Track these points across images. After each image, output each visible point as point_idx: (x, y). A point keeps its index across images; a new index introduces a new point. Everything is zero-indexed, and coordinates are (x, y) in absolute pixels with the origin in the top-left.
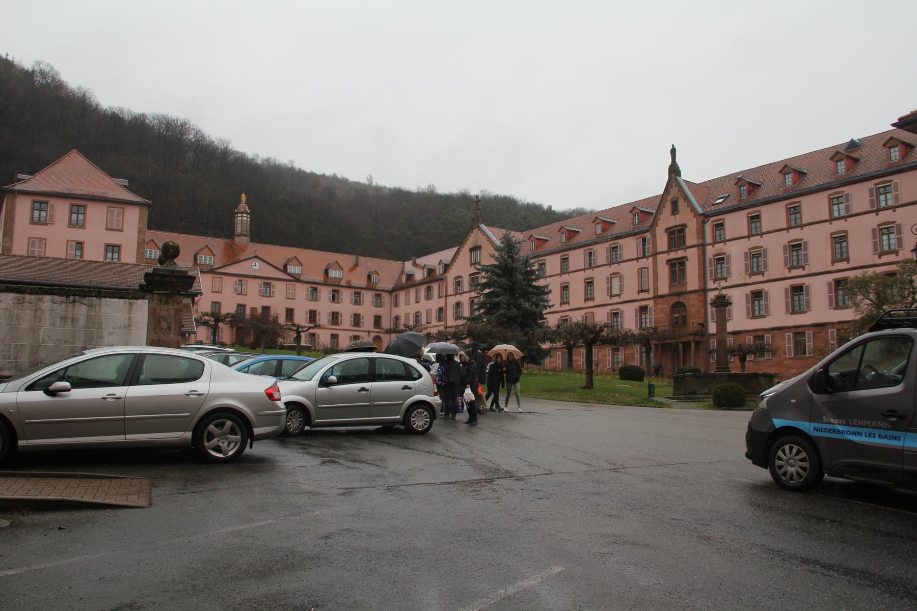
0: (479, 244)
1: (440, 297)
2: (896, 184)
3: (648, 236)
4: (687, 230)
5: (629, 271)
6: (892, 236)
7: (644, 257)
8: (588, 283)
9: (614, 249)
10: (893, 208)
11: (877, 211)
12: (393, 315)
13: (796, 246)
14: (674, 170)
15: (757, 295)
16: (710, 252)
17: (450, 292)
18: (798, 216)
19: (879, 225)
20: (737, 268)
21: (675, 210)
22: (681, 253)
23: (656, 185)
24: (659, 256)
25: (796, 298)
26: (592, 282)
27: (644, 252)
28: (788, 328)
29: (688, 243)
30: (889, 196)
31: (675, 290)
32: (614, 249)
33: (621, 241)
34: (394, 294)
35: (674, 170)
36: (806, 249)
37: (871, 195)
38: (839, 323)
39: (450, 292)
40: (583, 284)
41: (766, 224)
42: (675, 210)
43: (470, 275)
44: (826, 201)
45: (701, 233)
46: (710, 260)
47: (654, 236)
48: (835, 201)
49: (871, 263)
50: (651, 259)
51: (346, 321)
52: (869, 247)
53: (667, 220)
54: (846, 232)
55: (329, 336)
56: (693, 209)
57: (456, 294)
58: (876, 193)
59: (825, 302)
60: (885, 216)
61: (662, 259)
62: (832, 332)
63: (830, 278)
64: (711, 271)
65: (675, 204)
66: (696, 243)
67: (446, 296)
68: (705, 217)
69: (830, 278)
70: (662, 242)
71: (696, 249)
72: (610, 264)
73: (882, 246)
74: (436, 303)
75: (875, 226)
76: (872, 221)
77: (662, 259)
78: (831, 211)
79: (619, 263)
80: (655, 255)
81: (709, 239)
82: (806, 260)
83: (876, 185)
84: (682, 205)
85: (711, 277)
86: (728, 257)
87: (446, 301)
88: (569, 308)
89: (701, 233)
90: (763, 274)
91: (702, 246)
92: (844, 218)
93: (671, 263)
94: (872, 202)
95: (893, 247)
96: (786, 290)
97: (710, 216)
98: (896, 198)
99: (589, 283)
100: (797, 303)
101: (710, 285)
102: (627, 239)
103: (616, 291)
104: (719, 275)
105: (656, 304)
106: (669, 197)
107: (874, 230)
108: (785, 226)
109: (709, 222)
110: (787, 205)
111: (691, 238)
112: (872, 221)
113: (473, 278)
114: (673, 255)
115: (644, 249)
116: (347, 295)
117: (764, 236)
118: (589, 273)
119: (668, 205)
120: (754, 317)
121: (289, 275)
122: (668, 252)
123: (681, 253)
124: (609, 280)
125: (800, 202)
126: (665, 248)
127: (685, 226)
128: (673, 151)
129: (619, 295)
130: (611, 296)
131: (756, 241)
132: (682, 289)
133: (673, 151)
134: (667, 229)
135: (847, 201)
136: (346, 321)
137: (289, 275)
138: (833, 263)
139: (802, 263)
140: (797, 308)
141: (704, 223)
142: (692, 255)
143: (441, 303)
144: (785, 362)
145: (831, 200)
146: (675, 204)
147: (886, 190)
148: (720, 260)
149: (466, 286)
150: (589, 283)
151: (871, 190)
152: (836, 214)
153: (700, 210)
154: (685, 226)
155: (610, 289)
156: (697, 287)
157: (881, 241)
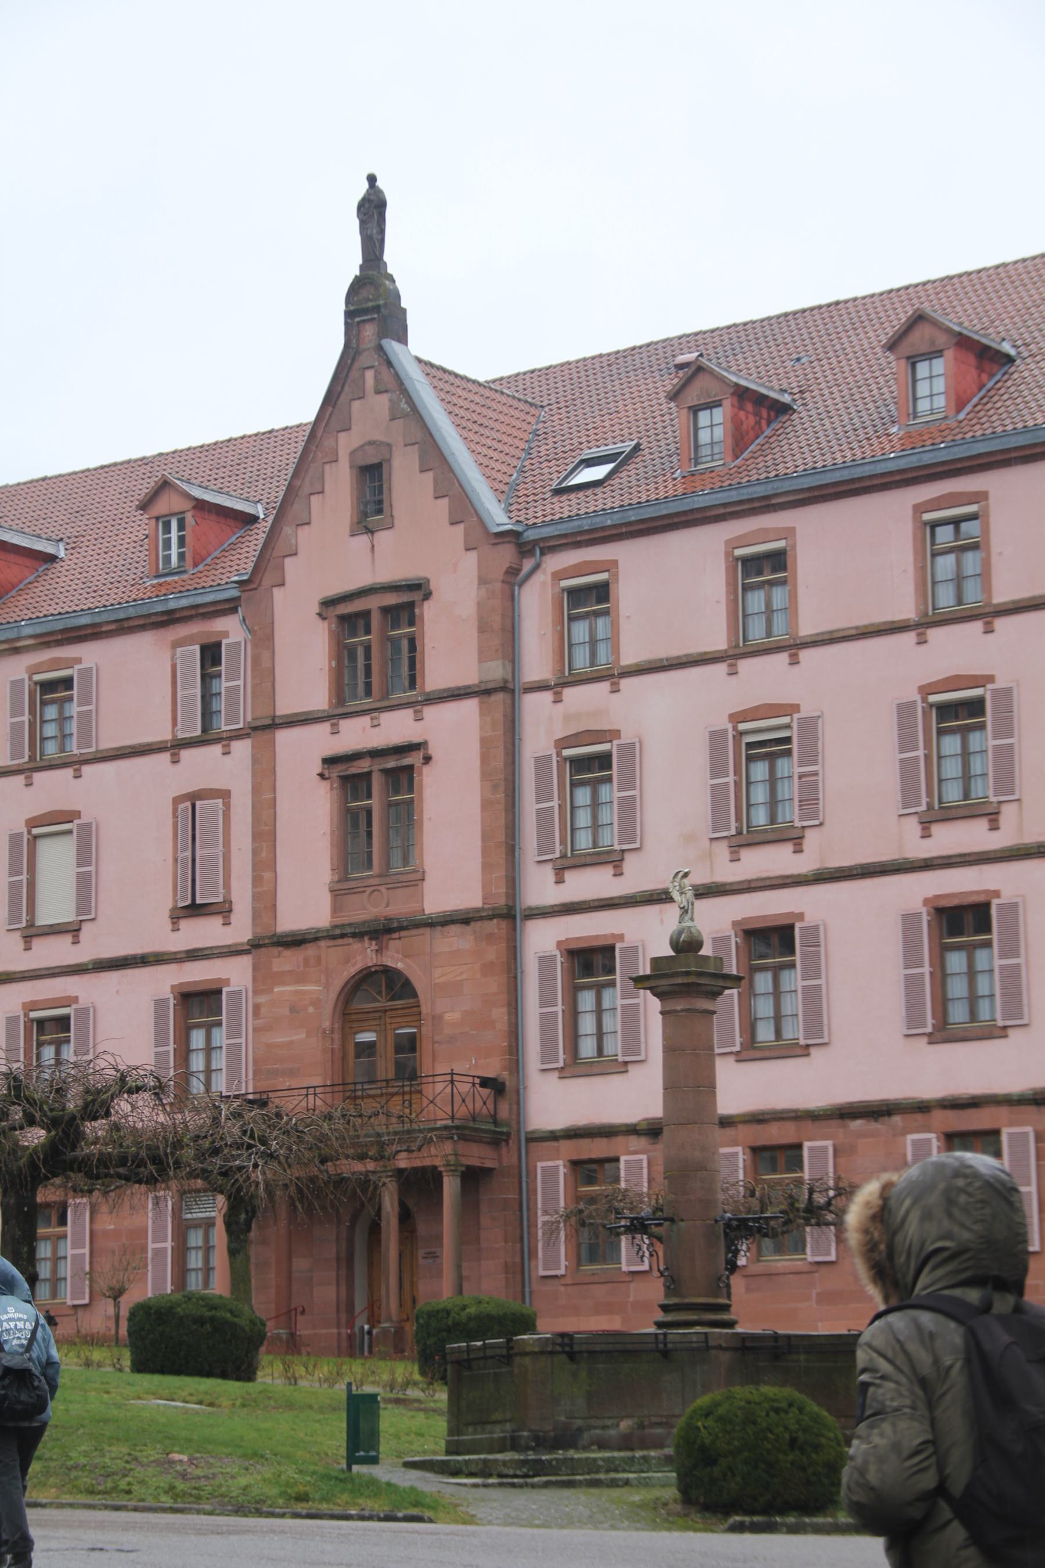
4: (429, 611)
14: (373, 307)
16: (544, 724)
22: (395, 727)
24: (283, 737)
25: (956, 961)
27: (208, 714)
29: (434, 679)
35: (373, 307)
45: (503, 634)
46: (542, 763)
47: (263, 637)
48: (944, 534)
50: (242, 749)
53: (329, 557)
56: (463, 509)
63: (917, 891)
64: (543, 816)
65: (372, 475)
68: (524, 547)
71: (471, 705)
77: (302, 751)
81: (537, 661)
82: (1006, 780)
84: (408, 485)
86: (629, 751)
89: (503, 634)
93: (348, 774)
96: (909, 921)
97: (550, 546)
100: (957, 988)
101: (540, 887)
103: (55, 905)
104: (584, 841)
105: (263, 979)
106: (346, 443)
110: (919, 509)
111: (450, 649)
114: (357, 734)
115: (207, 697)
119: (339, 486)
120: (943, 1033)
122: (332, 717)
123: (395, 727)
126: (319, 699)
127: (420, 588)
128: (372, 209)
129: (72, 931)
130: (32, 933)
132: (398, 906)
133: (372, 209)
134: (328, 603)
141: (514, 578)
142: (453, 736)
146: (372, 475)
154: (420, 588)
156: (469, 896)
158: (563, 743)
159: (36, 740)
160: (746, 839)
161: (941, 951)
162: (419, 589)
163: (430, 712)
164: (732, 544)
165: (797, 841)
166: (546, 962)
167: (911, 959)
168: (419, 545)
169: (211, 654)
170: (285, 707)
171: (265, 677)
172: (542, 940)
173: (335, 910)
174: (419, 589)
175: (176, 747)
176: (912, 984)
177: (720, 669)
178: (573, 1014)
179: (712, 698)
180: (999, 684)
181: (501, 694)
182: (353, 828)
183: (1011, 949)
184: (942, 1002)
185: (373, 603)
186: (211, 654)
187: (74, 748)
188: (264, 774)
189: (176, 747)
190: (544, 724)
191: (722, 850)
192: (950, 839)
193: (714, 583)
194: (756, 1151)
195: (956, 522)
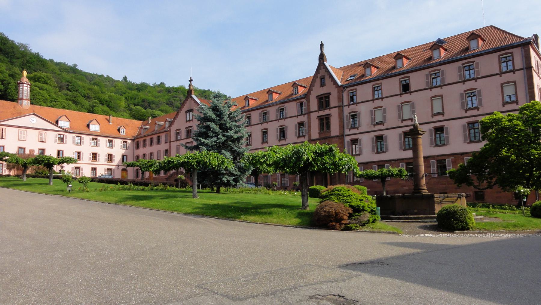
0: (192, 108)
1: (166, 143)
2: (477, 64)
3: (304, 101)
4: (331, 96)
5: (391, 104)
6: (474, 98)
7: (302, 114)
8: (264, 132)
9: (281, 110)
10: (475, 79)
11: (464, 82)
12: (135, 155)
13: (471, 93)
14: (322, 57)
15: (380, 138)
16: (347, 111)
17: (173, 139)
18: (380, 92)
19: (465, 91)
20: (365, 122)
21: (322, 85)
22: (322, 113)
23: (310, 70)
24: (311, 114)
25: (379, 143)
26: (266, 132)
27: (302, 112)
28: (402, 160)
29: (332, 106)
30: (472, 71)
31: (322, 136)
32: (281, 110)
33: (286, 105)
34: (136, 141)
35: (322, 57)
36: (359, 117)
37: (460, 71)
38: (438, 156)
39: (173, 139)
40: (261, 133)
41: (359, 97)
42: (322, 85)
43: (176, 130)
44: (496, 60)
45: (340, 99)
46: (347, 116)
47: (308, 101)
48: (376, 89)
49: (460, 116)
50: (306, 116)
51: (102, 158)
52: (458, 105)
53: (318, 91)
54: (267, 129)
55: (90, 169)
56: (335, 82)
57: (177, 140)
58: (374, 89)
59: (461, 138)
60: (470, 85)
61: (314, 116)
62: (433, 162)
63: (431, 126)
64: (347, 123)
65: (322, 78)
66: (337, 105)
67: (170, 142)
68: (344, 87)
69: (431, 126)
70: (314, 104)
71: (337, 108)
72: (278, 120)
73: (467, 104)
74: (163, 146)
75: (462, 92)
76: (461, 88)
77: (314, 116)
78: (374, 95)
79: (285, 119)
80: (309, 113)
81: (346, 102)
82: (359, 124)
83: (463, 64)
84: (327, 80)
85: (348, 126)
86: (359, 114)
87: (170, 144)
88: (384, 127)
89: (340, 99)
90: (357, 128)
91: (340, 107)
92: (440, 86)
93: (320, 118)
94: (427, 83)
95: (475, 105)
96: (373, 139)
97: (347, 87)
98: (443, 80)
99: (265, 133)
100: (379, 147)
101: (347, 132)
102: (290, 103)
103: (406, 116)
104: (301, 134)
106: (319, 76)
107: (462, 95)
108: (399, 93)
109: (346, 91)
110: (400, 79)
111: (334, 102)
112: (461, 88)
113: (189, 131)
114: (322, 113)
115: (301, 109)
116: (103, 141)
117: (516, 72)
118: (265, 126)
119: (318, 80)
120: (378, 153)
121: (60, 127)
122: (318, 111)
123: (327, 112)
124: (400, 108)
125: (409, 77)
126: (316, 109)
127: (330, 94)
128: (322, 45)
129: (442, 113)
130: (403, 121)
131: (282, 122)
132: (328, 135)
133: (322, 45)
134: (317, 96)
135: (443, 75)
136: (102, 158)
137: (60, 127)
138: (432, 117)
139: (357, 125)
140: (438, 143)
141: (342, 91)
142: (334, 113)
143: (166, 146)
144: (400, 182)
145: (373, 88)
146: (322, 78)
147: (436, 75)
148: (354, 116)
149: (183, 134)
150: (265, 133)
151: (459, 68)
152: (376, 97)
153: (340, 84)
154: (330, 94)
155: (400, 115)
156: (337, 133)
157: (467, 101)
158: (349, 113)
159: (177, 138)
160: (299, 137)
161: (435, 134)
162: (329, 94)
163: (331, 110)
164: (373, 85)
165: (383, 124)
166: (348, 142)
167: (373, 143)
168: (328, 88)
169: (302, 104)
170: (311, 110)
171: (309, 106)
172: (347, 139)
173: (319, 136)
174: (329, 94)
175: (297, 116)
176: (373, 146)
177: (399, 96)
178: (377, 145)
179: (260, 127)
180: (478, 89)
181: (340, 107)
182: (321, 125)
183: (386, 141)
184: (405, 145)
185: (323, 96)
186: (302, 104)
187: (284, 117)
188: (309, 118)
189: (297, 116)
190: (347, 111)
191: (373, 126)
192: (470, 113)
193: (370, 90)
194: (437, 161)
195: (378, 87)
